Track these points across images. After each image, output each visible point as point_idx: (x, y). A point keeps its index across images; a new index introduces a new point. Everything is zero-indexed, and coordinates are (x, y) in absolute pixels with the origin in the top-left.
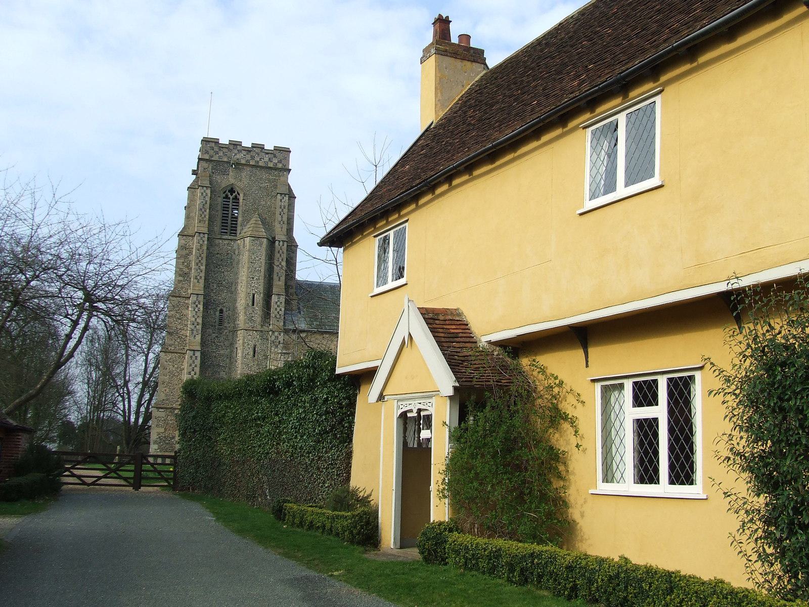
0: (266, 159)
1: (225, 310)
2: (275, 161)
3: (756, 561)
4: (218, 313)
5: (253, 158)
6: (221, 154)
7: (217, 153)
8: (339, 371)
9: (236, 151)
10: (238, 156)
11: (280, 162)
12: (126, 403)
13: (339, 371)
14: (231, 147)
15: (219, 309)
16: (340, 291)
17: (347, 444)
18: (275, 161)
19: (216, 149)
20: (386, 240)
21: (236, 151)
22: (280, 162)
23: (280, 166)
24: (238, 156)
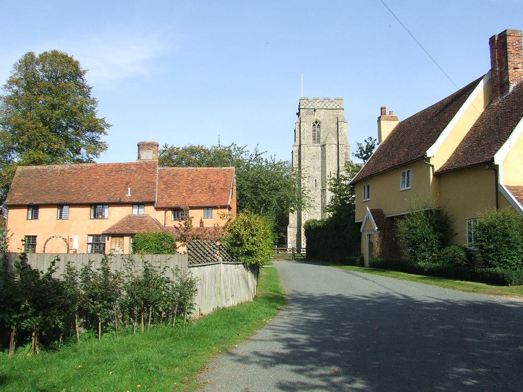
0: (332, 105)
1: (317, 180)
2: (336, 105)
3: (201, 222)
4: (314, 182)
5: (325, 105)
6: (310, 105)
7: (307, 105)
8: (356, 222)
9: (317, 103)
10: (318, 105)
11: (338, 105)
12: (406, 177)
13: (356, 222)
14: (314, 101)
15: (314, 179)
16: (30, 236)
17: (196, 216)
18: (336, 105)
19: (307, 103)
20: (404, 173)
21: (317, 103)
22: (338, 105)
23: (338, 107)
24: (318, 105)
